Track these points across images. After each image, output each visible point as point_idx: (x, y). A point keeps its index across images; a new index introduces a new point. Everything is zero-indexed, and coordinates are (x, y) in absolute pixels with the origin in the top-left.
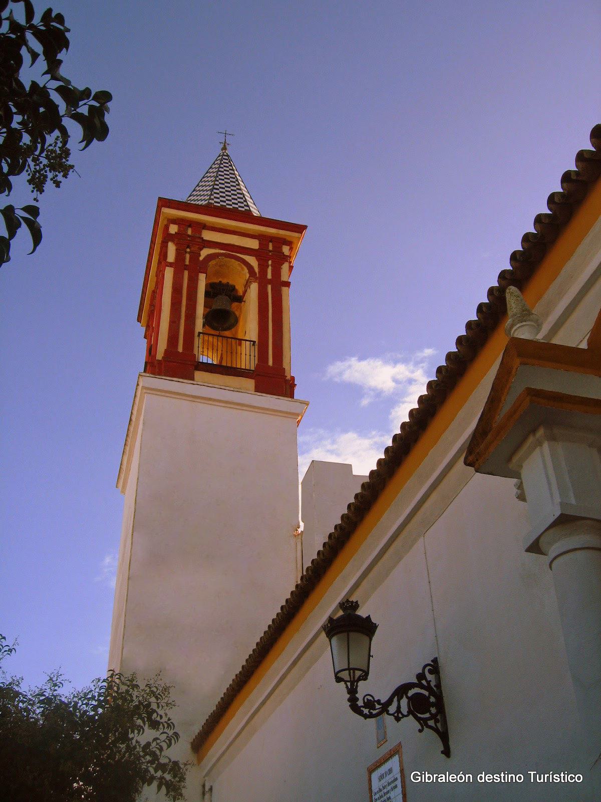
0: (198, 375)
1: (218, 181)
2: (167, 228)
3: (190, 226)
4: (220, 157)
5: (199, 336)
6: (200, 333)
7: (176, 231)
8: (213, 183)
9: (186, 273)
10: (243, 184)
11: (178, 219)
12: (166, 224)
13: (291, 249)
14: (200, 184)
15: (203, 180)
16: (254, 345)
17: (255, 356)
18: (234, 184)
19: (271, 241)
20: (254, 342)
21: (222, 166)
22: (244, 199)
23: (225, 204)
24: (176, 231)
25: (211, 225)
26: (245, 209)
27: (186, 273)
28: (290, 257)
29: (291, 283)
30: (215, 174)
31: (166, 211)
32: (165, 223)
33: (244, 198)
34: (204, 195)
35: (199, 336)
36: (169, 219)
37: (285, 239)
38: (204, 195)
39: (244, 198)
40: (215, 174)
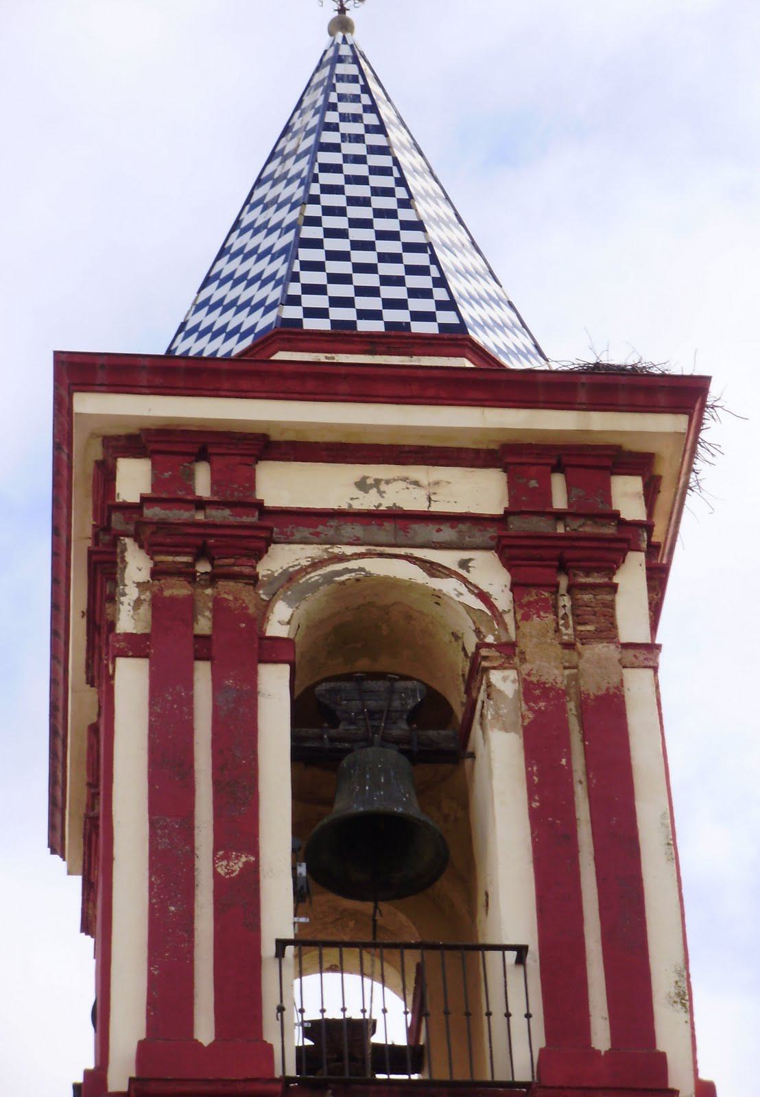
0: (298, 960)
1: (334, 127)
2: (105, 476)
3: (202, 455)
4: (325, 72)
5: (280, 953)
6: (281, 944)
7: (147, 490)
8: (295, 214)
9: (203, 673)
10: (417, 161)
11: (147, 431)
12: (100, 457)
13: (651, 493)
14: (247, 219)
15: (258, 194)
16: (521, 960)
17: (528, 1016)
18: (388, 203)
19: (558, 468)
20: (522, 951)
21: (332, 117)
22: (434, 272)
23: (347, 314)
24: (147, 490)
25: (290, 436)
26: (442, 327)
27: (203, 673)
28: (648, 527)
29: (663, 649)
30: (303, 164)
31: (87, 404)
32: (97, 452)
33: (433, 269)
34: (261, 280)
35: (280, 953)
36: (117, 438)
37: (618, 449)
38: (261, 280)
39: (433, 269)
40: (303, 164)
